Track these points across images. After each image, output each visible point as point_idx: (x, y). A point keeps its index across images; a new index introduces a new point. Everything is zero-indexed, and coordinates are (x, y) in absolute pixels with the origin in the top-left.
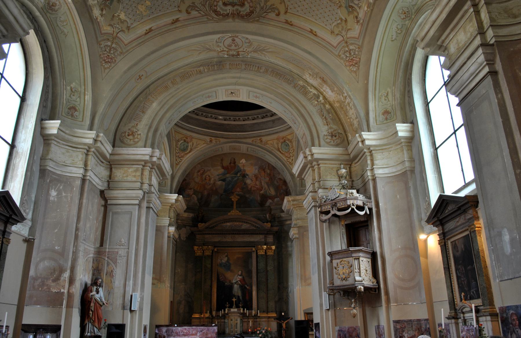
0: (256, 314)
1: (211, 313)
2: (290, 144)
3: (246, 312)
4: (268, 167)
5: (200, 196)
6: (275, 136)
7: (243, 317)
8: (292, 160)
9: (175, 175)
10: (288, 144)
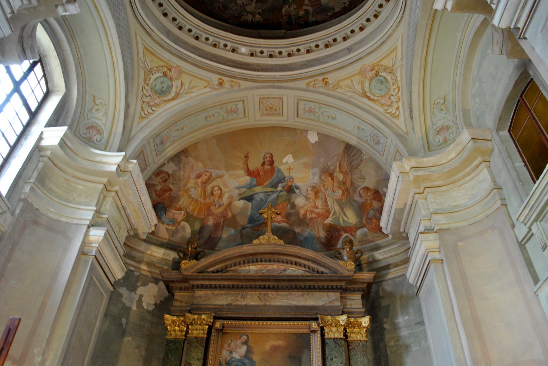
2: (389, 78)
4: (340, 168)
5: (197, 226)
6: (357, 67)
8: (398, 109)
9: (135, 135)
10: (385, 78)
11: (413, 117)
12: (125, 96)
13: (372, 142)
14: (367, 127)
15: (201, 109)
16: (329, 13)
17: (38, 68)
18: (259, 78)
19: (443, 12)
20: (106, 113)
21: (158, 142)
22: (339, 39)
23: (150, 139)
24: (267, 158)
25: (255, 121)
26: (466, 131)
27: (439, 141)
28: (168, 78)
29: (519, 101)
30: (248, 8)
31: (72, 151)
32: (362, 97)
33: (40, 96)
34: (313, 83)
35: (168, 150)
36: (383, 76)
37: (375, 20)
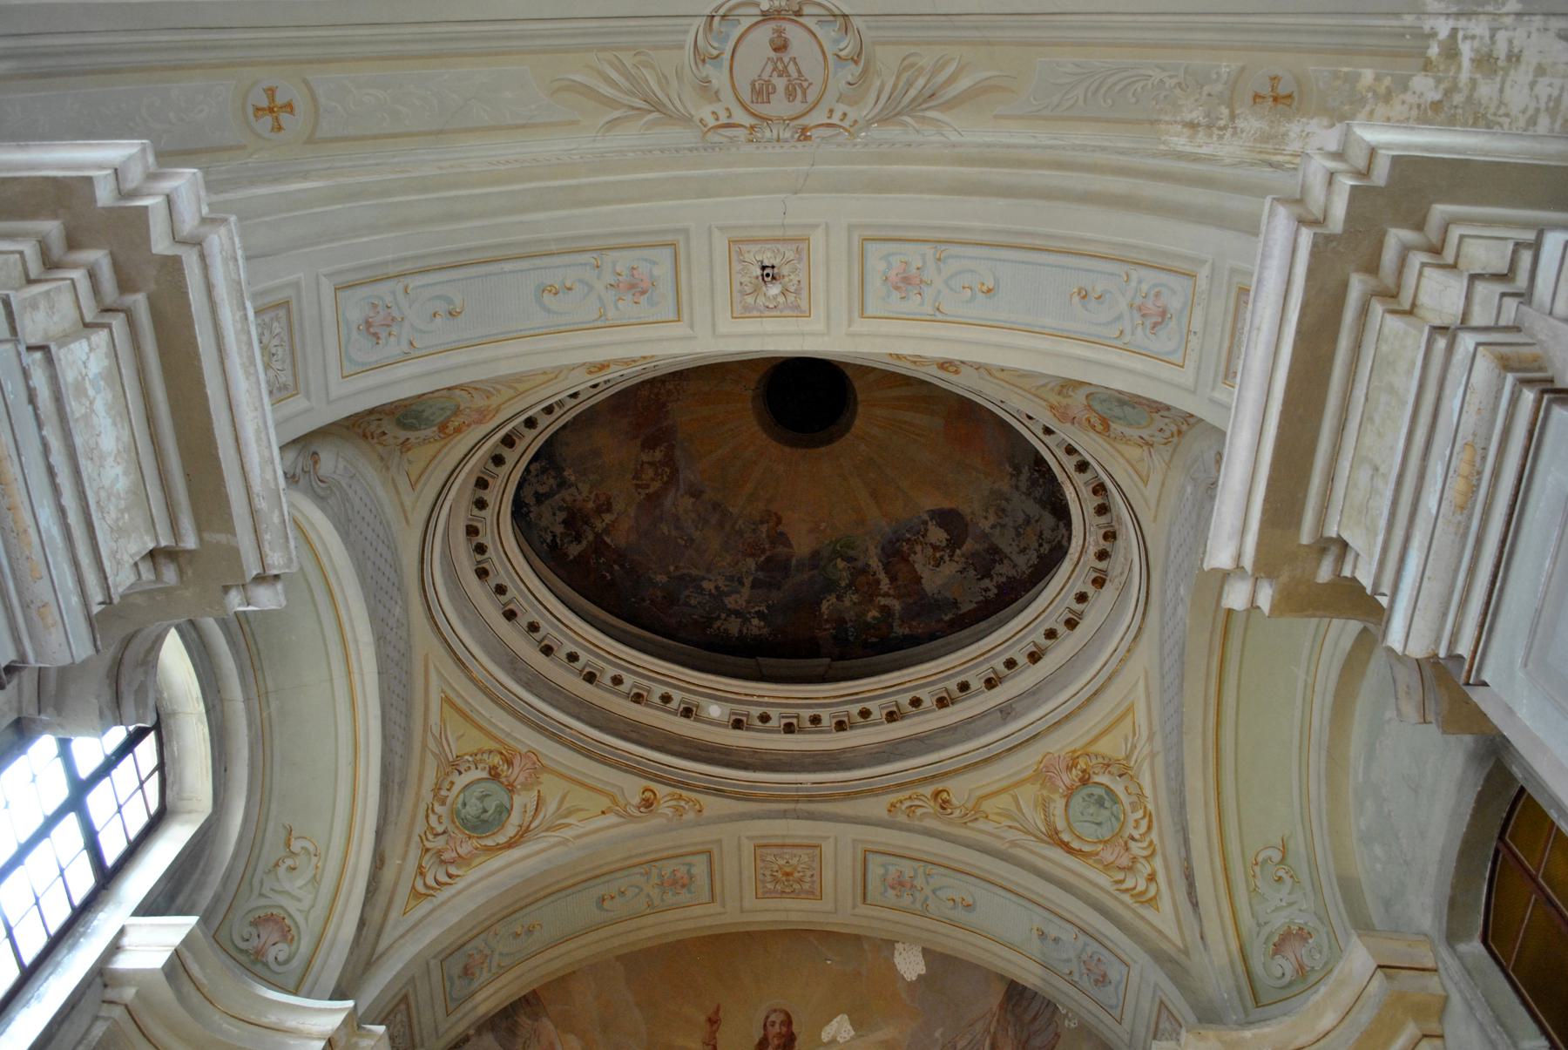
2: (1118, 788)
6: (1027, 760)
8: (1152, 878)
9: (391, 946)
10: (1109, 790)
11: (1197, 902)
12: (377, 832)
13: (1085, 976)
14: (1068, 934)
15: (589, 875)
16: (946, 615)
17: (147, 750)
18: (755, 788)
19: (1248, 618)
20: (315, 880)
21: (456, 970)
22: (976, 684)
23: (432, 962)
24: (773, 1024)
25: (742, 912)
26: (1358, 942)
27: (1283, 974)
28: (502, 783)
29: (1497, 852)
30: (730, 602)
31: (198, 989)
32: (1049, 843)
33: (137, 821)
34: (908, 803)
35: (480, 997)
36: (1102, 784)
37: (1068, 635)
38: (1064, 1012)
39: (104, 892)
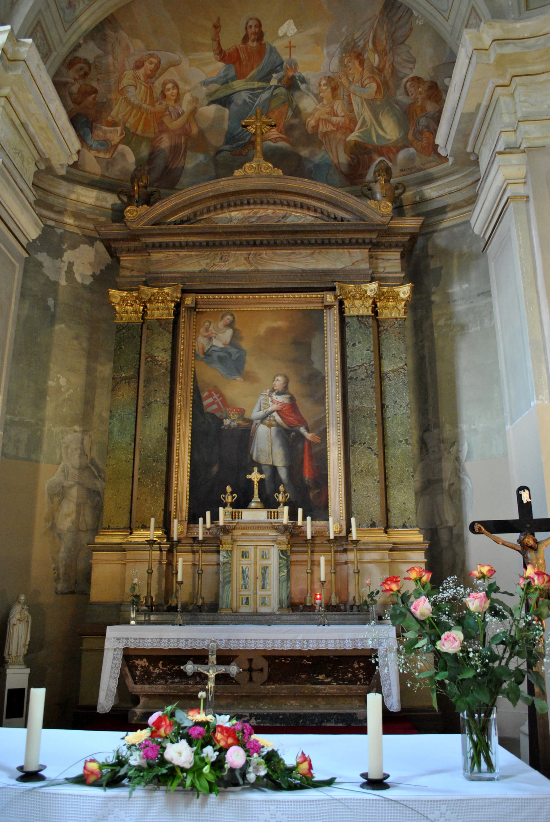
0: (344, 534)
1: (166, 527)
3: (304, 519)
4: (374, 43)
5: (145, 152)
7: (291, 544)
24: (251, 27)
35: (82, 19)
38: (416, 15)
39: (284, 385)
